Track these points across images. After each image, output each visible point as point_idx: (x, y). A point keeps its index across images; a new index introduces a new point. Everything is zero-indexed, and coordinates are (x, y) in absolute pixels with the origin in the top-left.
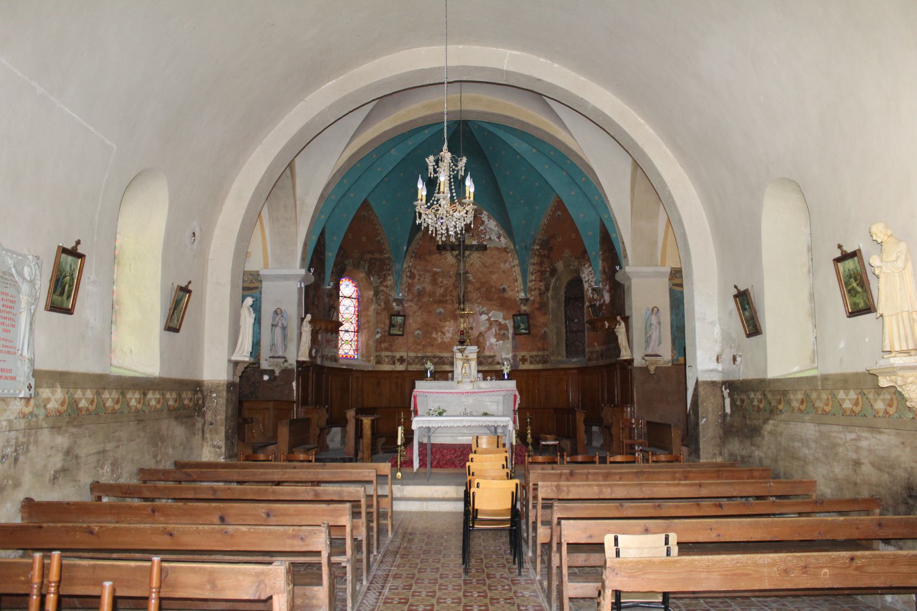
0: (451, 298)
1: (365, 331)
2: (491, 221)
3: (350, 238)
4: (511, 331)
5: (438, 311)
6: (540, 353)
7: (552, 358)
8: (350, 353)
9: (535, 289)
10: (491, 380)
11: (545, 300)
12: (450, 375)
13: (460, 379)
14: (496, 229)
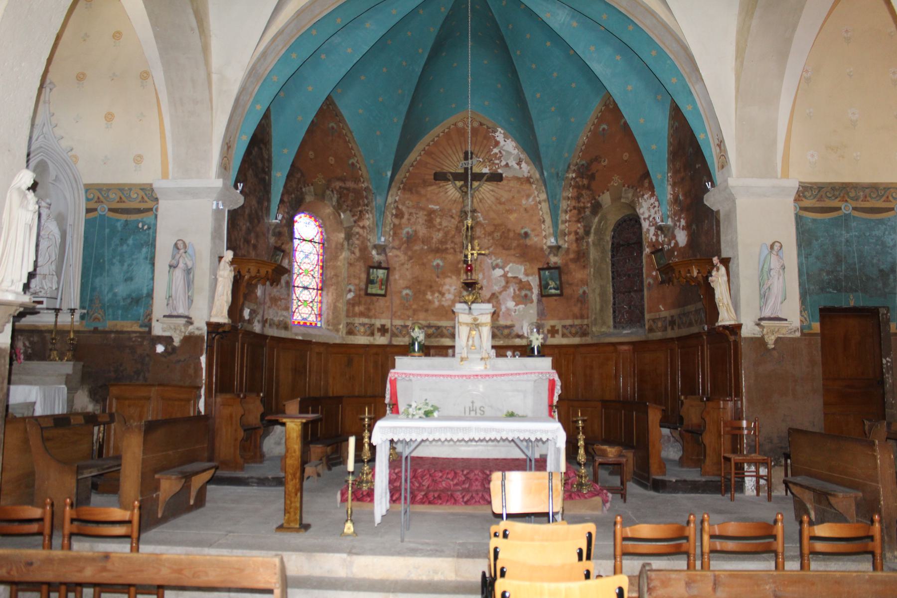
0: (452, 245)
1: (332, 289)
2: (509, 141)
3: (312, 157)
4: (536, 291)
5: (435, 264)
6: (577, 322)
7: (594, 329)
8: (310, 319)
9: (570, 233)
10: (514, 356)
11: (584, 247)
12: (450, 351)
13: (464, 355)
14: (516, 152)
